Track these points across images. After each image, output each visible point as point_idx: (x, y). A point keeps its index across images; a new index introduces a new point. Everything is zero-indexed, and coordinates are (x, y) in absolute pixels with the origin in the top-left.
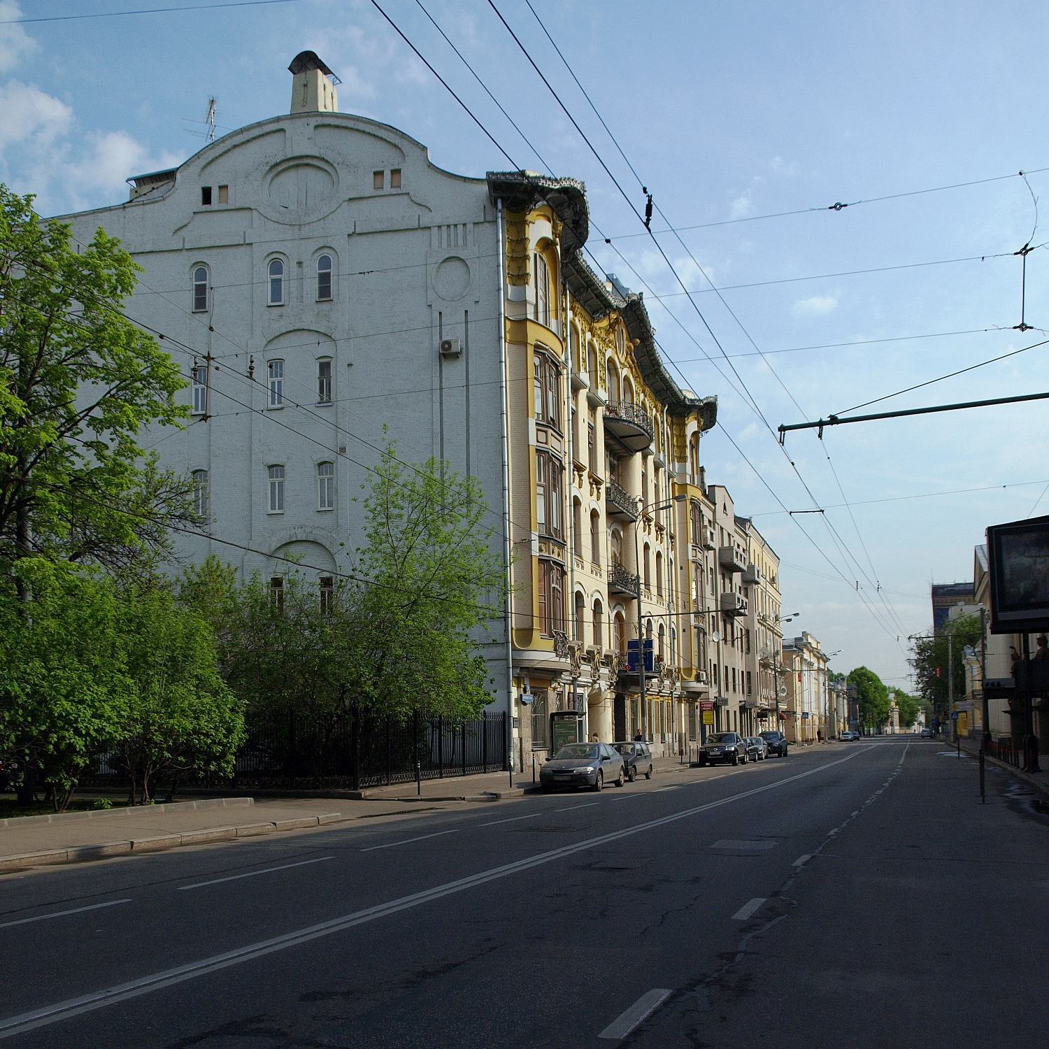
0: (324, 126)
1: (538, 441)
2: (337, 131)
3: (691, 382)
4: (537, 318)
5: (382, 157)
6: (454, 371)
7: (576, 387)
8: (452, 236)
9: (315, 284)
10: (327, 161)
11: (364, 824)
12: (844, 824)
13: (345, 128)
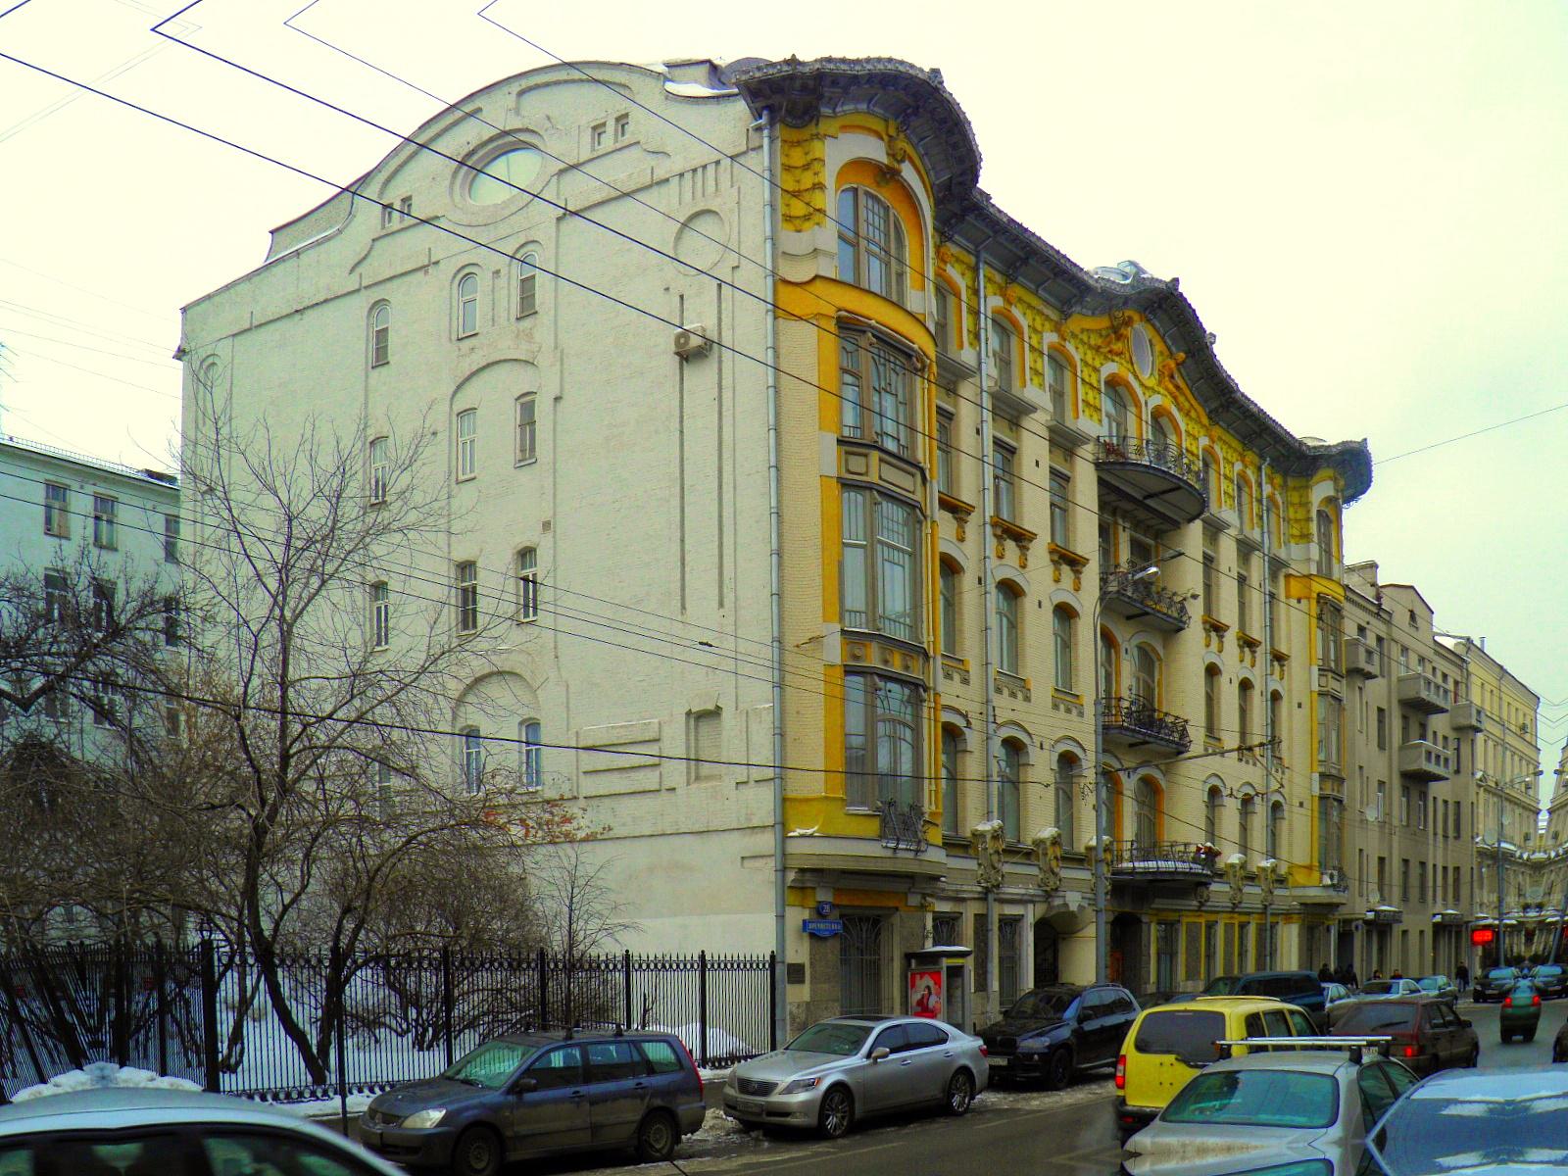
0: (530, 89)
1: (880, 478)
2: (548, 90)
3: (1306, 416)
4: (889, 291)
5: (600, 104)
6: (700, 378)
7: (1010, 411)
8: (699, 184)
9: (516, 299)
10: (533, 131)
11: (49, 1119)
12: (248, 938)
13: (557, 83)
